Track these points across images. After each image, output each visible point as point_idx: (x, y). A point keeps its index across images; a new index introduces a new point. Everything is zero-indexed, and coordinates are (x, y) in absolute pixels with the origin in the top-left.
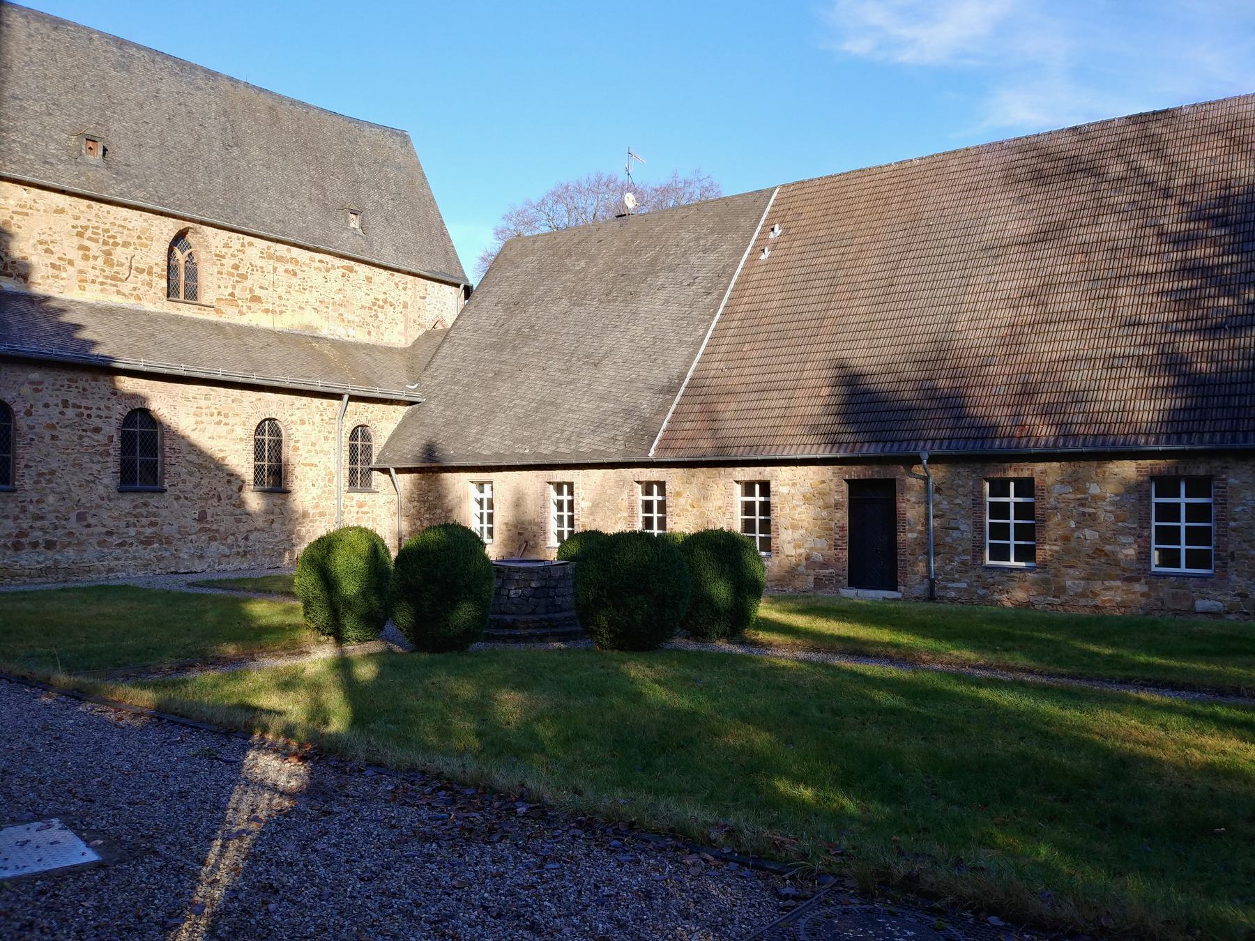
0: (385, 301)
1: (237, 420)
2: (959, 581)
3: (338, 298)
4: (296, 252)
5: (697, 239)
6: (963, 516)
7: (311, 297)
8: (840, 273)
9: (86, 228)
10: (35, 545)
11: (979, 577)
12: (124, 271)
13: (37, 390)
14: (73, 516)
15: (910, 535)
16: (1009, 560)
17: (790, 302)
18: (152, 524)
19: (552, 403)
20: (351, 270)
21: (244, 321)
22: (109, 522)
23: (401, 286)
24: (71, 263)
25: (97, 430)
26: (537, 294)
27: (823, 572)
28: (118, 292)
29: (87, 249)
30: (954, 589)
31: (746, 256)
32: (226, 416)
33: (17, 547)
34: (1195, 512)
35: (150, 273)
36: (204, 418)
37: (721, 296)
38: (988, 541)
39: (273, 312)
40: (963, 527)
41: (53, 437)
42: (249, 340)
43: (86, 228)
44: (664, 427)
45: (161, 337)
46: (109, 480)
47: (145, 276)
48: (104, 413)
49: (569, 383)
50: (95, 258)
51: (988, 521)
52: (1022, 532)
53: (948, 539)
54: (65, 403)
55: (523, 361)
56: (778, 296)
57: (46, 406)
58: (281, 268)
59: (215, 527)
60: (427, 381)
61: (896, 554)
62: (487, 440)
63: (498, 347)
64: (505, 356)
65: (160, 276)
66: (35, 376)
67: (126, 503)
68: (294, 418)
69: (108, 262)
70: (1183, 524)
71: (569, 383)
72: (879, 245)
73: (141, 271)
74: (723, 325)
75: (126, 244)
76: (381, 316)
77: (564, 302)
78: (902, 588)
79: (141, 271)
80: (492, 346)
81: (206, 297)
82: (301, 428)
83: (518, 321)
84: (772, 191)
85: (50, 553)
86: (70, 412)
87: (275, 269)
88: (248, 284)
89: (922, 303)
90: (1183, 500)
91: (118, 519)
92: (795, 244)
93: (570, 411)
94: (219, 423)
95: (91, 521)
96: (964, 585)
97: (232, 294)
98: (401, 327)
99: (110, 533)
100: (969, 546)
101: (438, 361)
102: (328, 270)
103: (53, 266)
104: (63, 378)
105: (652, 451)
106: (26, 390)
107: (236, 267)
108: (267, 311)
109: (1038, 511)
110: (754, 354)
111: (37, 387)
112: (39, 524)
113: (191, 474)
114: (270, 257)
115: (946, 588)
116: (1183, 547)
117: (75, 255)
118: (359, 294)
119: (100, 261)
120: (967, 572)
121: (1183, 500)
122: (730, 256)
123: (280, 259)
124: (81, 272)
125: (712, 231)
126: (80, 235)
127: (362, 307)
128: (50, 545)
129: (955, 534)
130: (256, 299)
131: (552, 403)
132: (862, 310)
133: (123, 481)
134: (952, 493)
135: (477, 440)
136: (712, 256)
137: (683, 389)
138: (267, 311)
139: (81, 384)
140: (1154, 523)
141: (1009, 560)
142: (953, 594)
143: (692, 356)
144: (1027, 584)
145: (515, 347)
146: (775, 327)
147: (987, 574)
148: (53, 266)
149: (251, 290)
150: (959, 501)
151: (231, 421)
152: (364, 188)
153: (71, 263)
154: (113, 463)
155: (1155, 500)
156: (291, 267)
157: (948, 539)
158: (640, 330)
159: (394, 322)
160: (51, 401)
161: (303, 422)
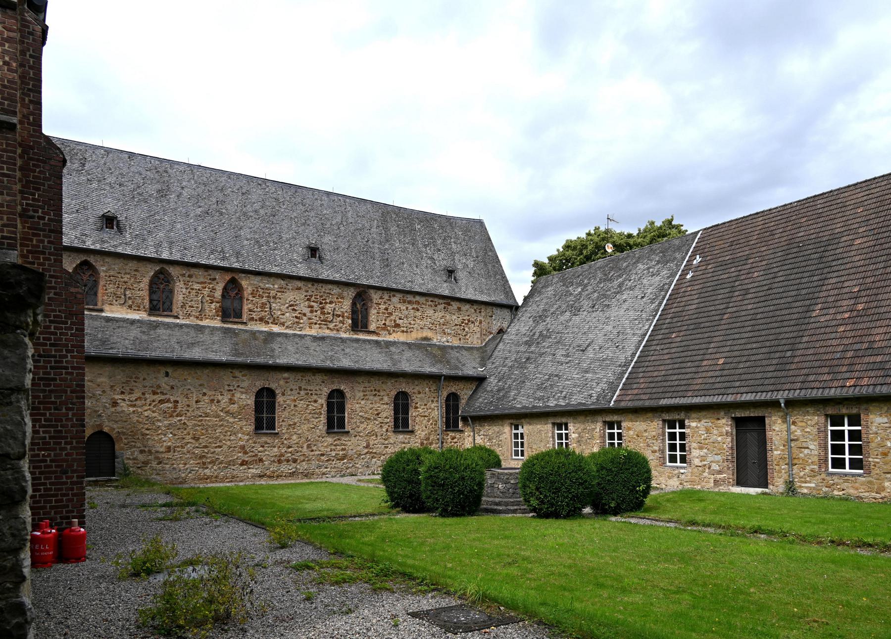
0: (469, 321)
1: (385, 393)
2: (810, 482)
3: (442, 321)
4: (418, 298)
5: (648, 269)
6: (811, 440)
7: (427, 322)
8: (737, 283)
9: (311, 296)
10: (288, 461)
11: (823, 479)
12: (330, 317)
13: (287, 382)
14: (305, 446)
15: (775, 452)
16: (833, 468)
17: (702, 305)
18: (343, 450)
19: (556, 376)
20: (449, 304)
21: (390, 338)
22: (322, 449)
23: (478, 311)
24: (305, 315)
25: (316, 401)
26: (552, 310)
27: (719, 476)
28: (328, 328)
29: (312, 307)
30: (807, 488)
31: (677, 277)
32: (379, 391)
33: (280, 462)
34: (854, 435)
35: (343, 317)
36: (367, 393)
37: (660, 303)
38: (830, 456)
39: (407, 332)
40: (811, 447)
41: (295, 406)
42: (393, 349)
43: (311, 296)
44: (620, 387)
45: (347, 350)
46: (322, 426)
47: (341, 318)
48: (319, 392)
49: (567, 363)
50: (316, 311)
51: (830, 442)
52: (854, 450)
53: (802, 455)
54: (300, 388)
55: (543, 351)
56: (696, 301)
57: (291, 390)
58: (410, 307)
59: (374, 451)
60: (489, 366)
61: (767, 465)
62: (519, 398)
63: (528, 344)
64: (533, 348)
65: (348, 318)
66: (286, 375)
67: (330, 440)
68: (415, 391)
69: (323, 313)
70: (847, 443)
71: (567, 363)
72: (764, 263)
73: (339, 316)
74: (661, 322)
75: (331, 303)
76: (467, 329)
77: (568, 314)
78: (771, 487)
79: (339, 316)
80: (526, 343)
81: (372, 327)
82: (419, 396)
83: (541, 327)
84: (699, 232)
85: (294, 465)
86: (302, 393)
87: (407, 308)
88: (392, 318)
89: (789, 300)
90: (846, 428)
91: (326, 447)
92: (710, 267)
93: (567, 379)
94: (375, 395)
95: (314, 448)
96: (813, 485)
97: (384, 324)
98: (478, 335)
99: (322, 455)
100: (816, 459)
101: (496, 353)
102: (436, 306)
103: (296, 317)
104: (299, 376)
105: (612, 403)
106: (282, 382)
107: (386, 309)
108: (403, 331)
109: (864, 436)
110: (679, 339)
111: (287, 380)
112: (290, 450)
113: (362, 423)
114: (404, 302)
115: (801, 487)
116: (847, 456)
117: (307, 311)
118: (454, 317)
119: (319, 312)
120: (815, 476)
121: (846, 428)
122: (668, 277)
123: (410, 302)
124: (310, 319)
125: (658, 262)
126: (308, 300)
127: (456, 325)
128: (295, 461)
129: (806, 451)
130: (397, 326)
131: (556, 376)
132: (750, 307)
133: (329, 428)
134: (804, 424)
135: (515, 399)
136: (658, 278)
137: (633, 364)
138: (403, 331)
139: (307, 378)
140: (667, 442)
141: (833, 468)
142: (805, 491)
143: (640, 342)
144: (857, 485)
145: (538, 343)
146: (693, 321)
147: (829, 478)
148: (296, 317)
149: (395, 321)
150: (808, 430)
151: (382, 394)
152: (457, 257)
153: (305, 315)
154: (323, 419)
155: (830, 428)
156: (415, 306)
157: (802, 455)
158: (610, 328)
159: (474, 332)
160: (294, 387)
161: (419, 393)
